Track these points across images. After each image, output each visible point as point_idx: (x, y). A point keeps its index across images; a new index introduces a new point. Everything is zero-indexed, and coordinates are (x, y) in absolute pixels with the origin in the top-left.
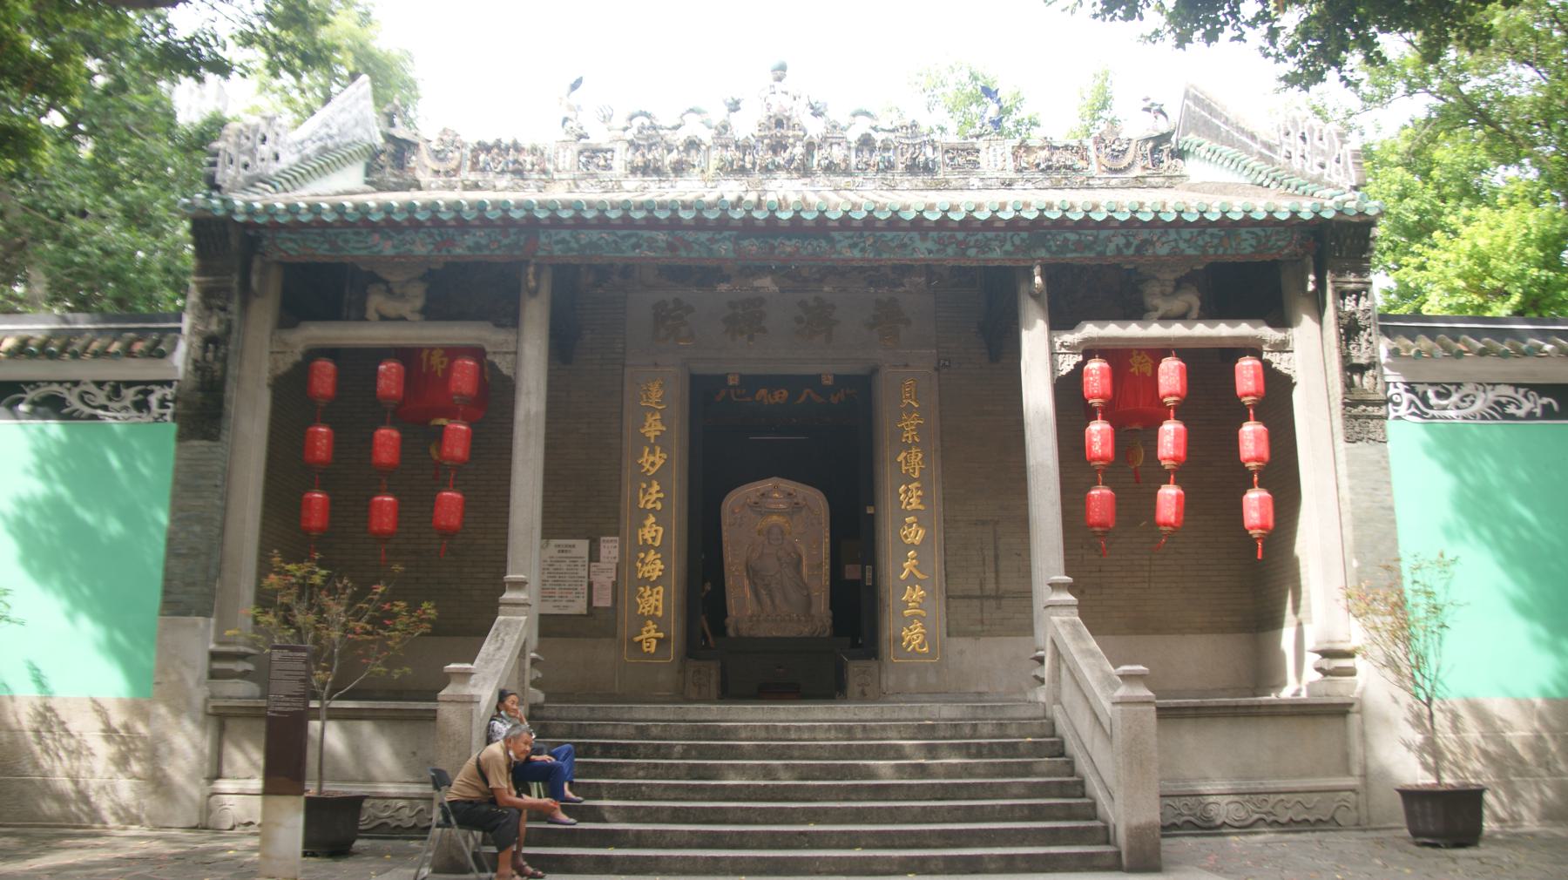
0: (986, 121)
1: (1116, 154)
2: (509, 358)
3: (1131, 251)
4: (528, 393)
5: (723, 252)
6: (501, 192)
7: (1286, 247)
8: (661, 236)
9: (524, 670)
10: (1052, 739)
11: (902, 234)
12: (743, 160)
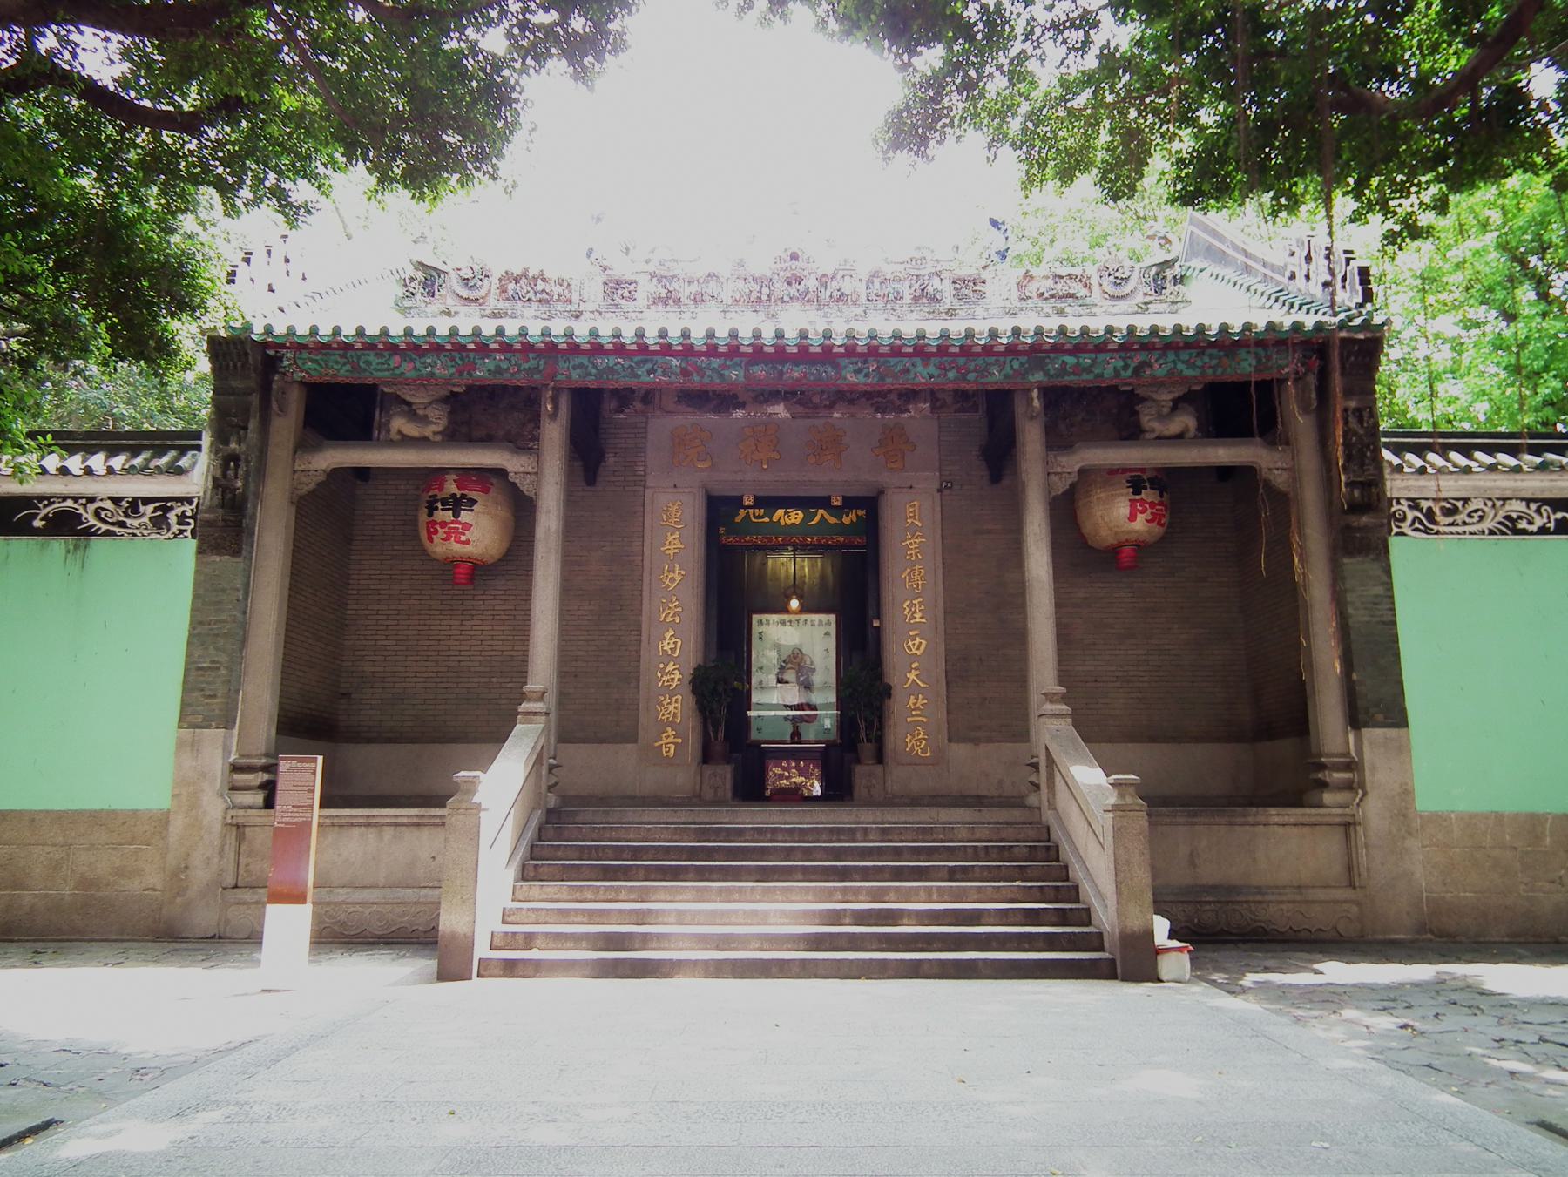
0: (993, 253)
1: (1118, 281)
2: (529, 478)
3: (1129, 372)
4: (549, 512)
5: (734, 377)
6: (529, 323)
7: (1287, 366)
8: (675, 362)
9: (541, 776)
10: (1074, 906)
11: (906, 359)
12: (760, 292)
